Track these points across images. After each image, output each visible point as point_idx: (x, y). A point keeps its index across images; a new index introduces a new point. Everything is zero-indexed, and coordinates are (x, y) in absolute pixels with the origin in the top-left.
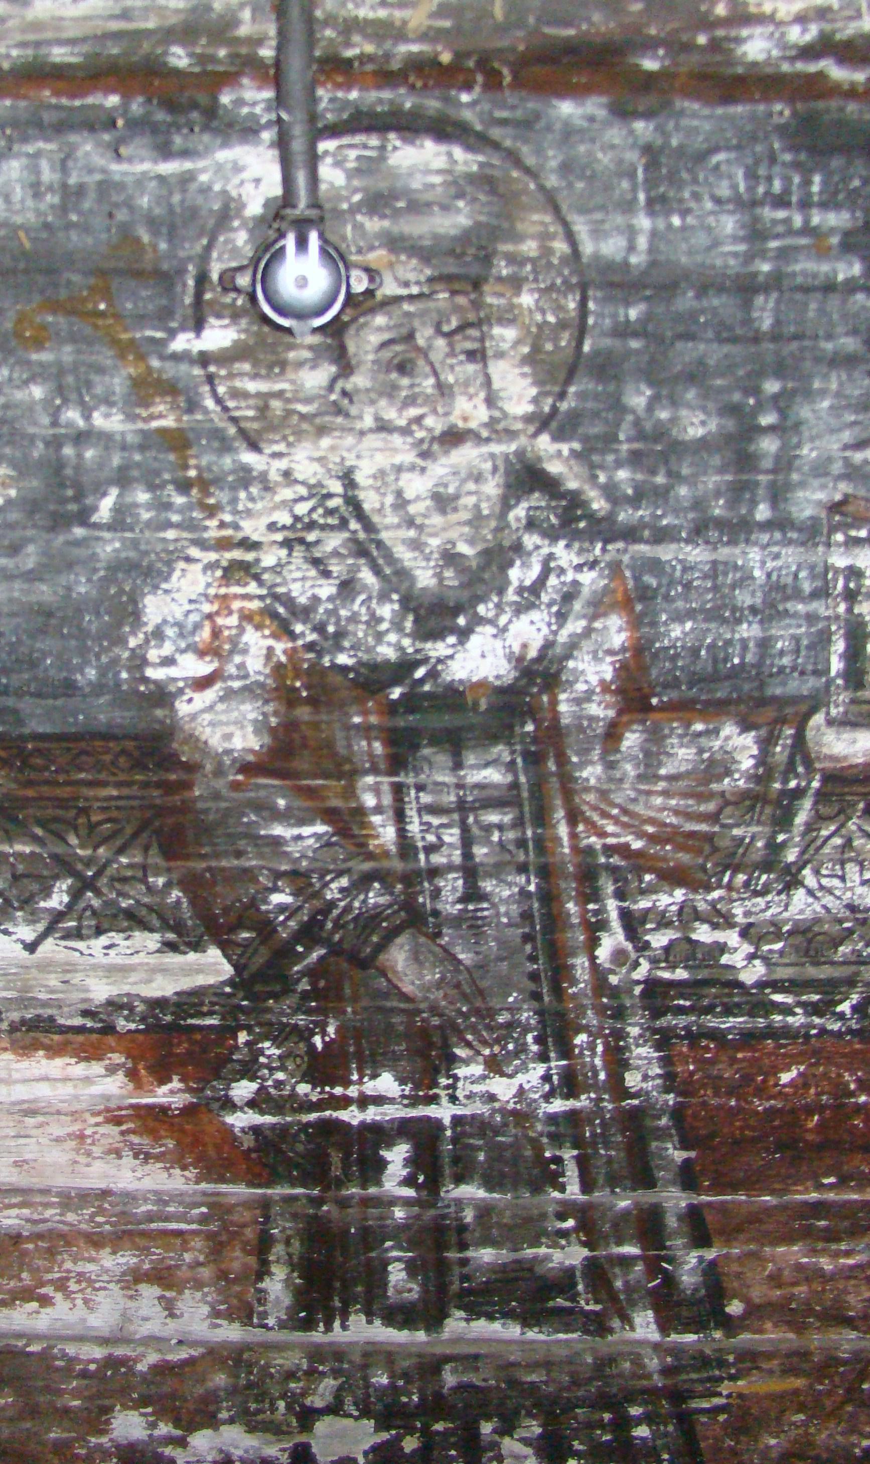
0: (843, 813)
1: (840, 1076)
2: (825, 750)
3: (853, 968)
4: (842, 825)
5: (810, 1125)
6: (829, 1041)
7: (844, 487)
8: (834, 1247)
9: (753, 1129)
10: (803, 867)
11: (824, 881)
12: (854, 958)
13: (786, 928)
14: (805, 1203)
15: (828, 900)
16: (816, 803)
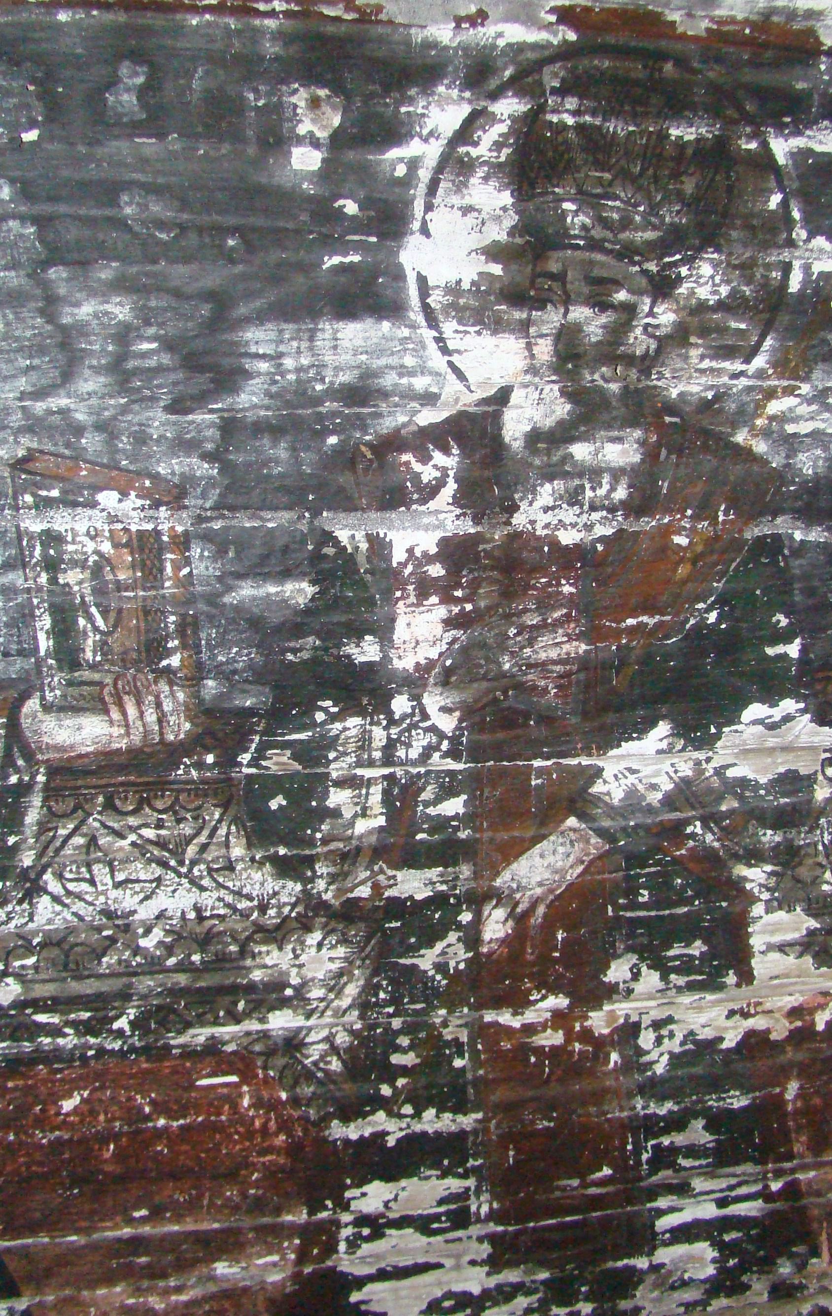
0: (81, 808)
1: (130, 1099)
2: (46, 739)
3: (125, 980)
4: (83, 822)
5: (107, 1155)
6: (112, 1062)
7: (28, 442)
8: (161, 1284)
9: (41, 1164)
10: (44, 870)
11: (71, 886)
12: (122, 969)
13: (36, 941)
14: (119, 1240)
15: (79, 907)
16: (45, 800)
